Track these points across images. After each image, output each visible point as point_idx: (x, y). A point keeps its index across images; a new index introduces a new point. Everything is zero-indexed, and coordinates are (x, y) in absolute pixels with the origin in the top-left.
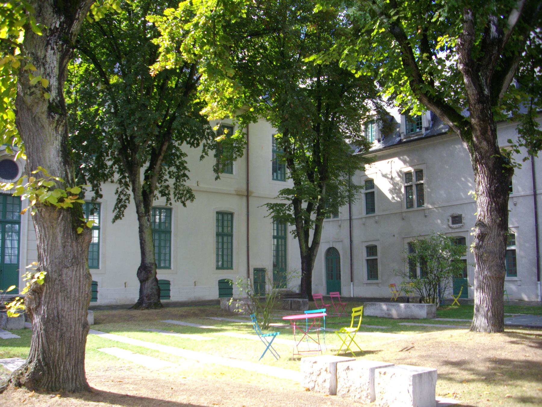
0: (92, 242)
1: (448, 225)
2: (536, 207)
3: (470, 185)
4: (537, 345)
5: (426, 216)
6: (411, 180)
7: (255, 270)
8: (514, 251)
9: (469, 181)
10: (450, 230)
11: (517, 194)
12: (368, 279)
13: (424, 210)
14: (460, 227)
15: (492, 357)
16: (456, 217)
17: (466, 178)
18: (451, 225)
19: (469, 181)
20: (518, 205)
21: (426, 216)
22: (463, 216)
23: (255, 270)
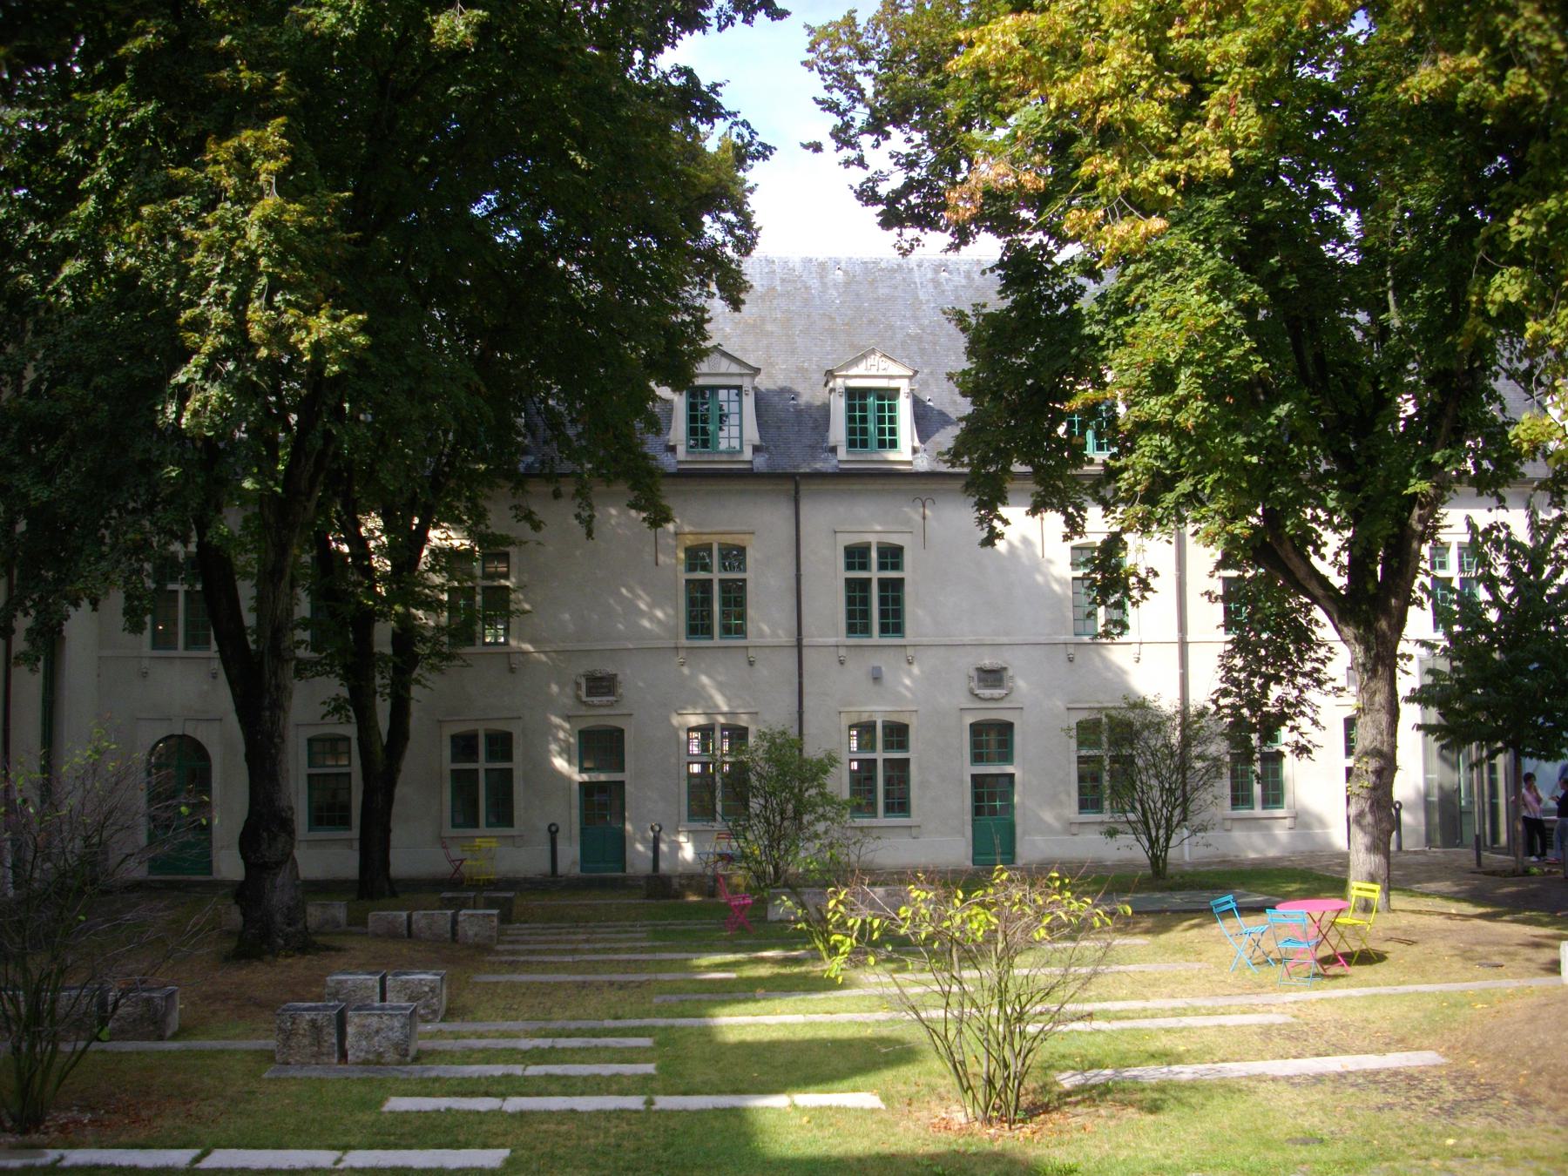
0: (296, 617)
1: (578, 697)
2: (800, 676)
3: (643, 606)
4: (319, 939)
5: (512, 670)
6: (864, 566)
7: (345, 822)
8: (1012, 776)
9: (640, 597)
10: (583, 711)
11: (760, 642)
12: (310, 830)
13: (508, 654)
14: (611, 705)
15: (1092, 1051)
16: (601, 679)
17: (630, 590)
18: (584, 699)
19: (640, 597)
20: (758, 666)
21: (512, 670)
22: (620, 677)
23: (345, 822)
